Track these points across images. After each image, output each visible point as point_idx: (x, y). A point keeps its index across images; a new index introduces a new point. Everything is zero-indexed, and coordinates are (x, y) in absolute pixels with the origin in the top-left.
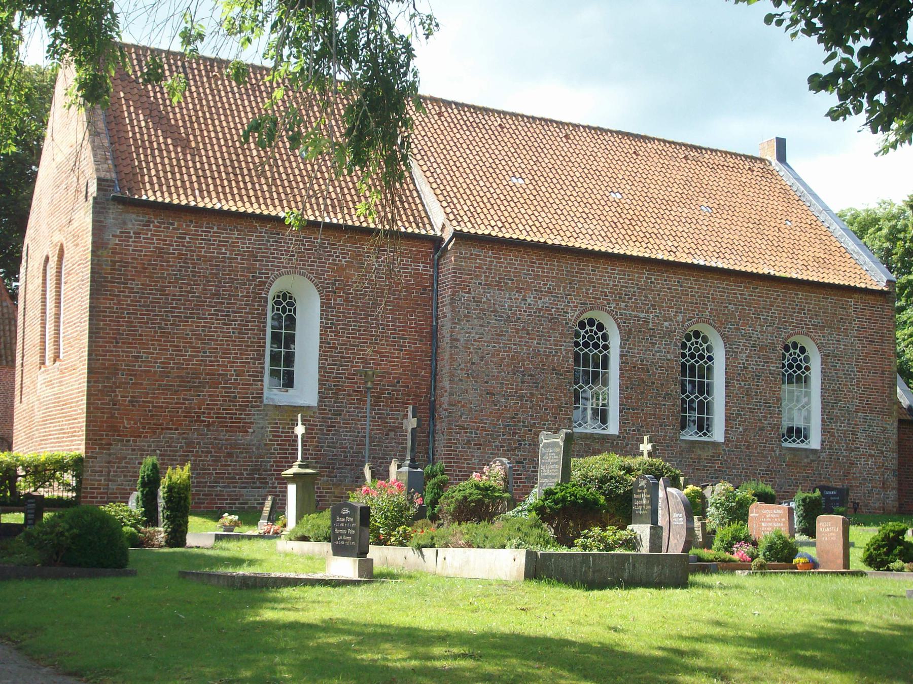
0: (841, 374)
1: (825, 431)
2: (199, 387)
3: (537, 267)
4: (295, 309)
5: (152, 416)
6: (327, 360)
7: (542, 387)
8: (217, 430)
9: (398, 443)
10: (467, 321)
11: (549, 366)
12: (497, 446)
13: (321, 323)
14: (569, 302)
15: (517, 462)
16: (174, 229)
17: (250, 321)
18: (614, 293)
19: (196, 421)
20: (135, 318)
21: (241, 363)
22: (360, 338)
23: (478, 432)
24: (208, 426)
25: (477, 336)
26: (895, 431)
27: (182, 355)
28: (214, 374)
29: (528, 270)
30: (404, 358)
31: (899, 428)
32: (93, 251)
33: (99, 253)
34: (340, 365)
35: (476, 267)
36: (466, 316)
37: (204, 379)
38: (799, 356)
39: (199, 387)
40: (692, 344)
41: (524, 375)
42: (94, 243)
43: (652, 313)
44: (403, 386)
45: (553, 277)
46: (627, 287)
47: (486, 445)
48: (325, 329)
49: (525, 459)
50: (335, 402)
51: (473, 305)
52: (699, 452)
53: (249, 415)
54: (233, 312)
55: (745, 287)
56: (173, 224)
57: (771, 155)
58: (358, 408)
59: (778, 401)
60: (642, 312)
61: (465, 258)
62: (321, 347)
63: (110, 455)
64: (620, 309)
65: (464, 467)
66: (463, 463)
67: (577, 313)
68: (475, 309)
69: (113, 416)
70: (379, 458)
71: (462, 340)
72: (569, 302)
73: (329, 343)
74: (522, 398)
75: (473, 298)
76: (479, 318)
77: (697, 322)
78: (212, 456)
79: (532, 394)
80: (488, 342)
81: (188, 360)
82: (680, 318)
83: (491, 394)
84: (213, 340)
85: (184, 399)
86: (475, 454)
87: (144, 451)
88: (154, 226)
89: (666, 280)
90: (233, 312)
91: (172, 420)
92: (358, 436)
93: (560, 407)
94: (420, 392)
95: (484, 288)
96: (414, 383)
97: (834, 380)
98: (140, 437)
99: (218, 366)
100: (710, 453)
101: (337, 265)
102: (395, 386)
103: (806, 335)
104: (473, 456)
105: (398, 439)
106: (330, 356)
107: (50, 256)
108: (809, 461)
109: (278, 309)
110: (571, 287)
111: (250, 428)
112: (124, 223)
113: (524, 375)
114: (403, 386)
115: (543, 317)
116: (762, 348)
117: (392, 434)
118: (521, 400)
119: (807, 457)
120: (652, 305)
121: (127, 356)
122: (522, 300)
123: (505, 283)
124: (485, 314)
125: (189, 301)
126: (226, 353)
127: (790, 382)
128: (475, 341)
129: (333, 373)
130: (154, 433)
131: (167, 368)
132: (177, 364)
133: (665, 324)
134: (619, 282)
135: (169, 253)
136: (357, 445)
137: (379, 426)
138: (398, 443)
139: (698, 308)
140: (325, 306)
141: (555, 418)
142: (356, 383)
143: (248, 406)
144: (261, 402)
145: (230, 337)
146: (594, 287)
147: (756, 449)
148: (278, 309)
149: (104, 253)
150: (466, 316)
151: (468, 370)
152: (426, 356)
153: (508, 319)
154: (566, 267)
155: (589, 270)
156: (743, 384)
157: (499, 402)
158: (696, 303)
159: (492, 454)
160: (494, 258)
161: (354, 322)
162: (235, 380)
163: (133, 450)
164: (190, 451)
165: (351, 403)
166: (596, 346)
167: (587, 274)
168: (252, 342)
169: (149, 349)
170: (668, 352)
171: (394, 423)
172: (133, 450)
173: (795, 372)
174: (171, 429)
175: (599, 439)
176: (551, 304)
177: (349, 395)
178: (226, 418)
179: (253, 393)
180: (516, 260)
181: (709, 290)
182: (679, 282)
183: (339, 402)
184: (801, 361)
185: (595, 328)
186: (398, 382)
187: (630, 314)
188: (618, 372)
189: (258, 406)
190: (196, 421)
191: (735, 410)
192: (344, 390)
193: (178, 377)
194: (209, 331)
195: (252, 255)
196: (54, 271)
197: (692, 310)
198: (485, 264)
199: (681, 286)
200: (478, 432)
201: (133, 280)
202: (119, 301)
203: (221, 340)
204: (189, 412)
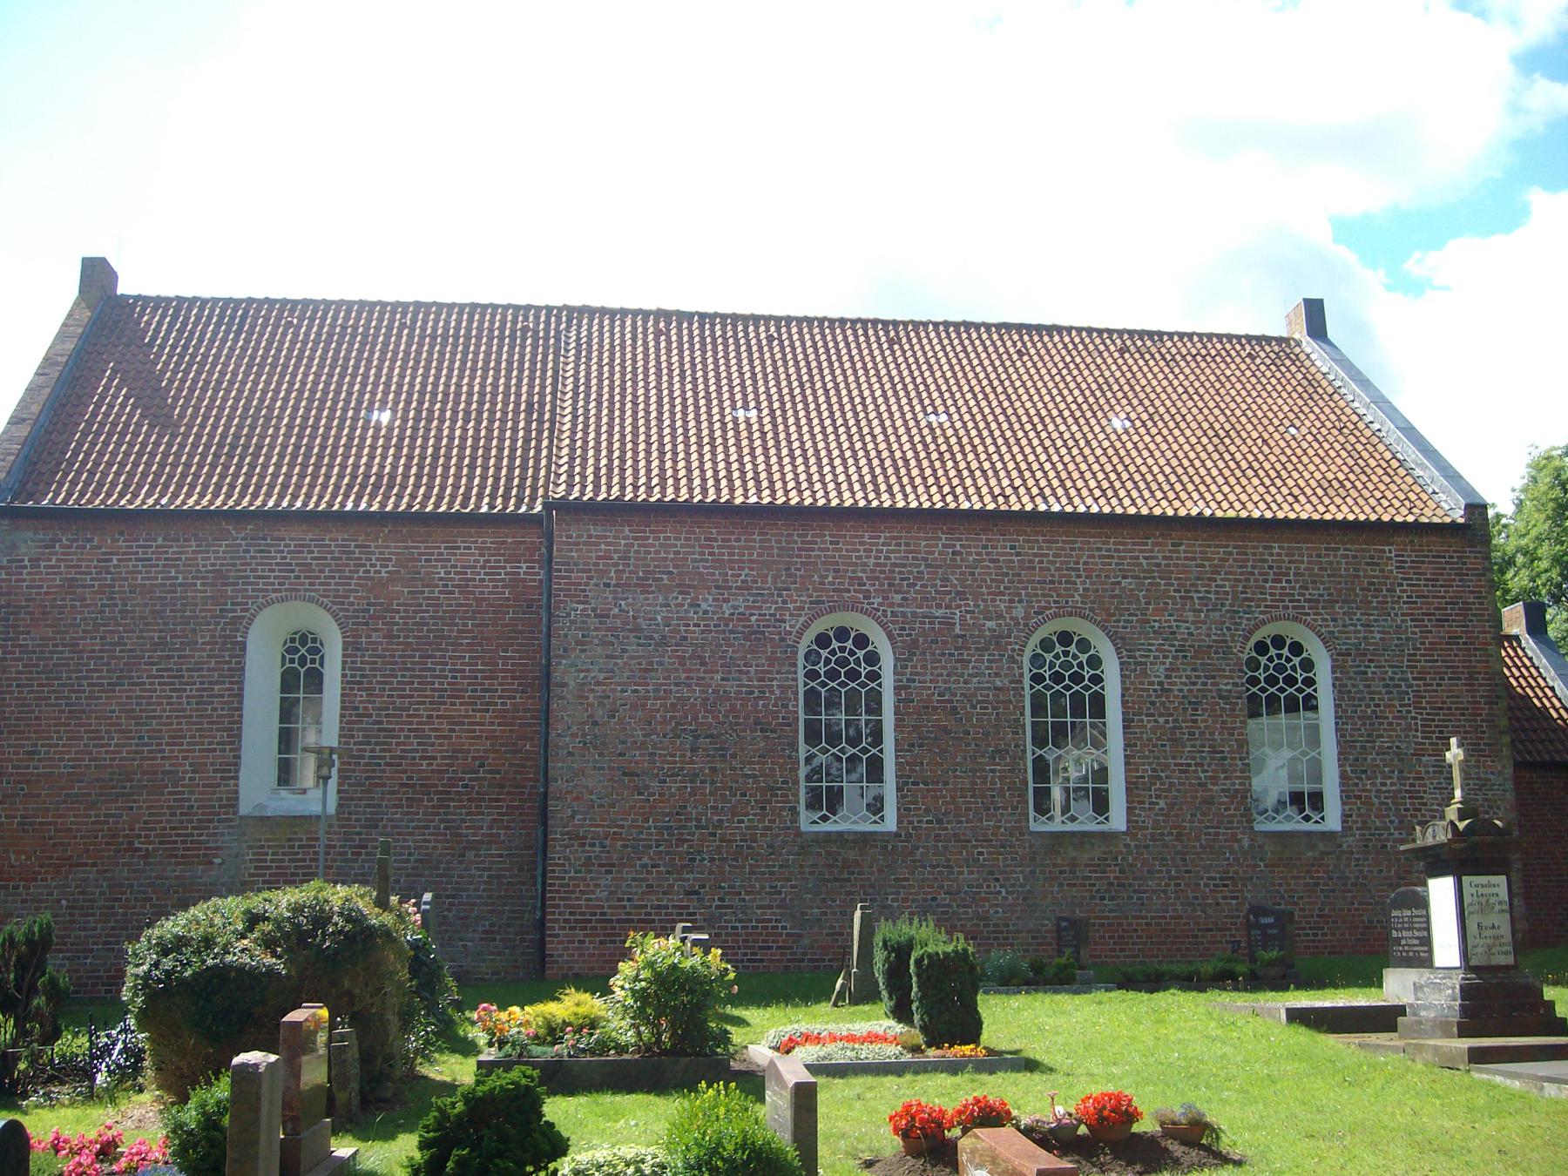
0: (1377, 686)
1: (1348, 795)
2: (132, 794)
3: (720, 547)
4: (322, 657)
5: (54, 845)
6: (353, 737)
7: (734, 756)
8: (161, 863)
9: (483, 869)
10: (582, 651)
11: (747, 718)
12: (645, 866)
13: (344, 676)
14: (785, 602)
15: (688, 893)
16: (93, 548)
17: (216, 683)
18: (878, 578)
19: (126, 850)
20: (30, 692)
21: (201, 751)
22: (411, 696)
23: (608, 842)
24: (146, 857)
25: (602, 676)
26: (1509, 785)
27: (103, 746)
28: (155, 773)
29: (702, 554)
30: (492, 724)
31: (1517, 780)
34: (377, 744)
35: (599, 558)
36: (578, 643)
37: (139, 780)
38: (1288, 660)
39: (132, 794)
40: (1057, 657)
41: (696, 737)
43: (959, 606)
44: (490, 772)
45: (751, 561)
46: (904, 566)
47: (623, 865)
49: (703, 886)
50: (368, 806)
51: (593, 622)
52: (1072, 853)
53: (215, 835)
54: (188, 670)
55: (1155, 544)
56: (91, 540)
57: (1300, 333)
58: (408, 813)
59: (1240, 746)
60: (939, 606)
61: (578, 544)
62: (342, 716)
64: (892, 605)
65: (580, 906)
66: (577, 899)
67: (802, 620)
68: (596, 629)
70: (448, 897)
71: (572, 683)
72: (785, 602)
73: (357, 708)
74: (693, 777)
75: (594, 610)
76: (604, 644)
77: (1056, 615)
78: (152, 906)
79: (713, 770)
80: (624, 684)
81: (113, 752)
82: (1019, 611)
83: (632, 774)
84: (154, 717)
85: (106, 816)
86: (602, 882)
87: (42, 901)
88: (62, 547)
89: (985, 547)
90: (188, 670)
91: (87, 851)
92: (408, 861)
93: (772, 789)
94: (524, 780)
95: (615, 592)
96: (511, 765)
97: (1364, 699)
98: (35, 879)
99: (163, 758)
100: (1097, 853)
101: (371, 579)
102: (477, 772)
103: (1295, 619)
104: (597, 886)
105: (483, 862)
106: (359, 730)
108: (1316, 854)
109: (292, 661)
110: (788, 576)
111: (216, 856)
112: (15, 546)
113: (696, 737)
114: (490, 772)
115: (731, 632)
116: (1199, 652)
118: (692, 781)
119: (1313, 847)
120: (958, 593)
121: (16, 753)
122: (690, 605)
123: (655, 579)
124: (617, 637)
125: (116, 658)
127: (1255, 714)
128: (598, 683)
129: (363, 757)
130: (58, 872)
131: (80, 766)
132: (95, 759)
133: (989, 624)
134: (887, 558)
135: (84, 586)
136: (408, 875)
137: (447, 841)
138: (483, 869)
139: (1055, 590)
141: (763, 808)
142: (405, 771)
143: (211, 821)
144: (235, 813)
145: (184, 710)
146: (835, 571)
147: (1198, 838)
148: (292, 661)
150: (578, 643)
151: (584, 735)
152: (533, 717)
153: (664, 642)
154: (778, 542)
155: (824, 542)
156: (1161, 720)
157: (647, 787)
158: (1052, 582)
159: (634, 880)
160: (636, 539)
161: (401, 670)
162: (191, 779)
164: (116, 900)
165: (395, 806)
166: (1077, 678)
167: (820, 549)
168: (220, 716)
169: (50, 738)
170: (997, 675)
171: (474, 835)
172: (24, 901)
173: (1282, 690)
174: (86, 865)
175: (854, 841)
176: (747, 607)
177: (394, 793)
178: (175, 842)
179: (221, 799)
180: (678, 539)
181: (1079, 557)
182: (1012, 547)
183: (374, 806)
184: (1294, 668)
185: (1285, 652)
186: (482, 765)
187: (914, 614)
189: (230, 820)
190: (126, 850)
191: (1146, 770)
192: (384, 785)
193: (97, 780)
194: (148, 704)
195: (219, 575)
197: (1043, 595)
198: (616, 551)
199: (1018, 554)
200: (608, 842)
201: (28, 633)
203: (169, 717)
204: (114, 836)
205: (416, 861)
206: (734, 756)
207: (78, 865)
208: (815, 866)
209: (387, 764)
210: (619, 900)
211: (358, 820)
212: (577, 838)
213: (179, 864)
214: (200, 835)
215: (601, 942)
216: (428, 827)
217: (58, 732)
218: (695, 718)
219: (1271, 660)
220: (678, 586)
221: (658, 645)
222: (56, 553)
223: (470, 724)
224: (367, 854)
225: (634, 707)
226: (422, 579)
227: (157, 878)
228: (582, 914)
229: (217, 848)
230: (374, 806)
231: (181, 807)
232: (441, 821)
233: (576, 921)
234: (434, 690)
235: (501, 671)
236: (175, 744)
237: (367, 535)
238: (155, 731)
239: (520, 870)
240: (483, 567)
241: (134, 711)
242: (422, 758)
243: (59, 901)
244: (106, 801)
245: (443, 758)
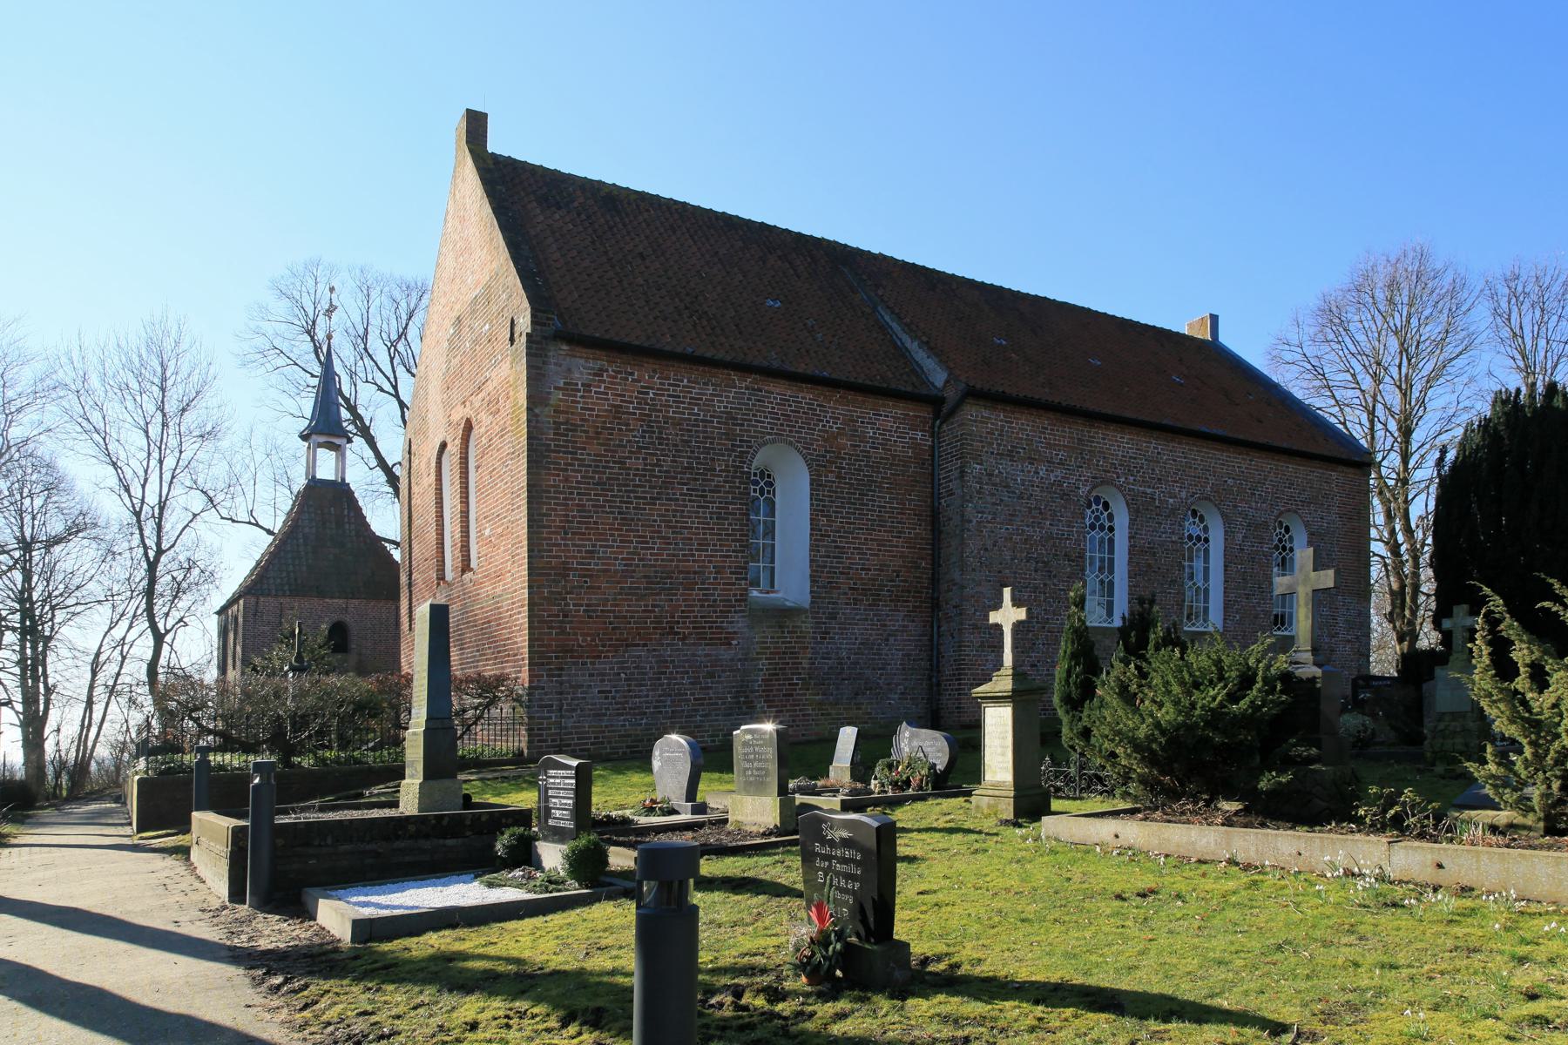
32: (528, 409)
33: (537, 411)
42: (529, 397)
48: (818, 511)
56: (632, 374)
63: (561, 683)
69: (563, 631)
82: (1183, 495)
107: (449, 441)
117: (892, 639)
126: (703, 545)
140: (815, 484)
149: (546, 413)
163: (591, 675)
166: (1102, 528)
188: (1126, 557)
196: (456, 459)
202: (566, 480)
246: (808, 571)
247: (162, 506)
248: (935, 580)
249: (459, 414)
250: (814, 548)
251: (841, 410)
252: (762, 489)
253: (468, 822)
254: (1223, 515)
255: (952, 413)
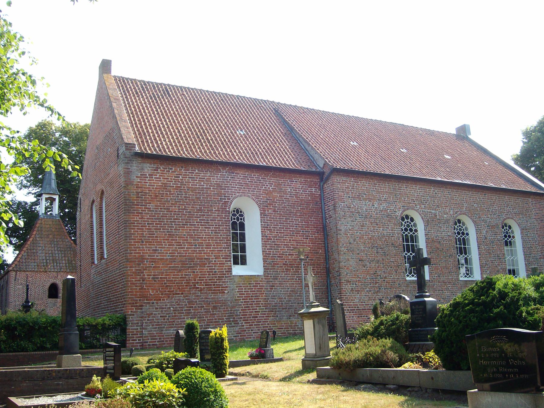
4: (244, 218)
7: (387, 255)
8: (206, 293)
12: (367, 291)
13: (262, 225)
16: (172, 172)
19: (193, 288)
20: (153, 226)
24: (201, 290)
25: (351, 227)
27: (182, 248)
28: (202, 259)
30: (309, 243)
34: (274, 249)
48: (264, 228)
50: (273, 271)
53: (224, 282)
56: (171, 169)
58: (286, 274)
61: (339, 183)
62: (262, 239)
64: (422, 208)
66: (350, 302)
67: (401, 212)
68: (348, 212)
69: (142, 288)
71: (343, 230)
73: (267, 237)
75: (346, 205)
76: (350, 217)
78: (204, 309)
81: (186, 251)
82: (451, 212)
84: (200, 238)
85: (185, 275)
86: (357, 297)
87: (163, 308)
88: (160, 171)
91: (179, 288)
92: (288, 291)
95: (351, 200)
98: (160, 300)
99: (204, 253)
103: (512, 218)
104: (355, 298)
106: (268, 244)
113: (377, 249)
118: (377, 263)
121: (149, 250)
125: (184, 214)
130: (169, 297)
131: (174, 256)
133: (445, 216)
136: (288, 296)
142: (284, 259)
143: (223, 277)
144: (231, 274)
148: (234, 219)
153: (366, 217)
157: (366, 265)
159: (365, 296)
160: (355, 182)
161: (280, 223)
164: (191, 307)
165: (282, 272)
172: (157, 308)
174: (179, 294)
177: (281, 267)
178: (211, 285)
183: (275, 272)
186: (307, 257)
190: (193, 288)
192: (278, 264)
194: (198, 233)
203: (205, 238)
205: (290, 291)
206: (387, 255)
207: (177, 294)
208: (410, 291)
209: (278, 257)
210: (362, 302)
211: (271, 277)
212: (349, 282)
213: (213, 293)
214: (220, 282)
215: (358, 317)
216: (293, 279)
217: (164, 242)
218: (377, 242)
219: (405, 223)
220: (368, 199)
221: (365, 218)
222: (159, 173)
223: (303, 243)
224: (275, 289)
225: (360, 238)
226: (283, 192)
227: (205, 298)
228: (352, 307)
229: (227, 287)
230: (275, 272)
231: (212, 272)
232: (297, 277)
233: (351, 310)
234: (290, 231)
235: (311, 225)
236: (208, 248)
237: (265, 174)
238: (201, 243)
239: (322, 294)
240: (302, 189)
241: (192, 235)
242: (289, 255)
243: (170, 308)
244: (184, 270)
245: (296, 255)
246: (262, 257)
247: (265, 378)
248: (327, 259)
249: (99, 187)
250: (264, 245)
251: (273, 180)
252: (238, 218)
253: (78, 372)
254: (473, 221)
255: (328, 179)
